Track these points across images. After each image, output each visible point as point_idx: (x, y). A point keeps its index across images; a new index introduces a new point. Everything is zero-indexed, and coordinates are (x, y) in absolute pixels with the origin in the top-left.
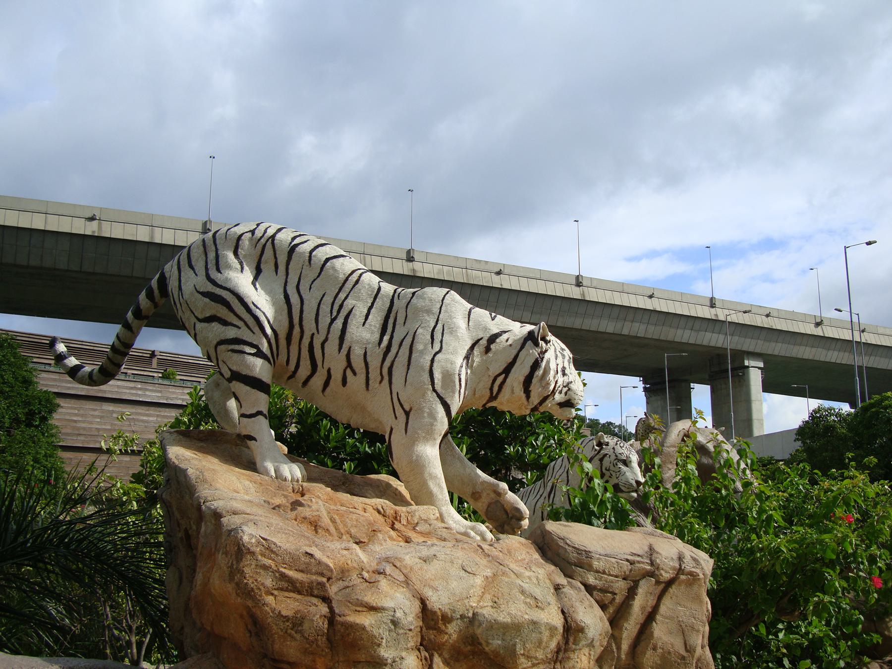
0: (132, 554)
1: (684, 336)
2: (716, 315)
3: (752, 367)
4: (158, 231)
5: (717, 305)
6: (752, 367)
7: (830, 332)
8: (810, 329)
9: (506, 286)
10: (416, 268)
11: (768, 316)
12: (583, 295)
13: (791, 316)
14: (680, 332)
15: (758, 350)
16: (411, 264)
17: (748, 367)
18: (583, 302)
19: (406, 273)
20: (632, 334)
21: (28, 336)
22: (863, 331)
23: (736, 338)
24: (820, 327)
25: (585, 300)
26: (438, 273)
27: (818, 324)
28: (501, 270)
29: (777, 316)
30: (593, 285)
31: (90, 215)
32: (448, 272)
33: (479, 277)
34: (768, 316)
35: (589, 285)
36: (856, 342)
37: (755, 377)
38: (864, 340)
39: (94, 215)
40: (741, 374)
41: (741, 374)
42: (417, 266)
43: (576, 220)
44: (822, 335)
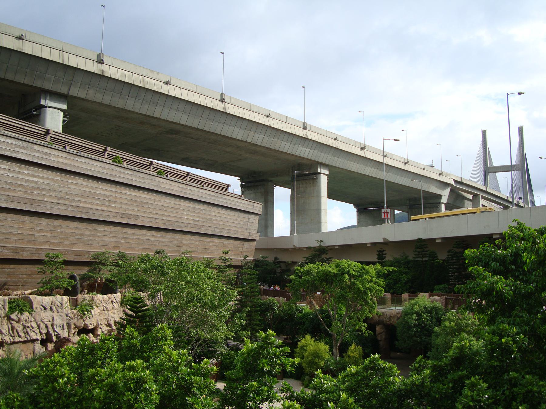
0: (143, 354)
1: (285, 147)
2: (307, 135)
3: (323, 174)
4: (66, 55)
5: (308, 128)
6: (323, 174)
7: (369, 155)
8: (358, 151)
9: (172, 94)
10: (104, 69)
11: (335, 139)
12: (225, 108)
13: (347, 141)
14: (226, 127)
15: (327, 163)
16: (100, 65)
17: (320, 173)
18: (101, 77)
19: (96, 72)
20: (254, 142)
21: (162, 166)
22: (385, 156)
23: (316, 152)
24: (363, 151)
25: (226, 113)
26: (121, 76)
27: (362, 149)
28: (168, 81)
29: (340, 140)
30: (232, 102)
31: (18, 34)
32: (129, 76)
33: (152, 84)
34: (335, 139)
35: (229, 102)
36: (385, 164)
37: (324, 181)
38: (385, 162)
39: (22, 35)
40: (315, 178)
41: (315, 178)
42: (105, 68)
43: (304, 86)
44: (364, 156)
